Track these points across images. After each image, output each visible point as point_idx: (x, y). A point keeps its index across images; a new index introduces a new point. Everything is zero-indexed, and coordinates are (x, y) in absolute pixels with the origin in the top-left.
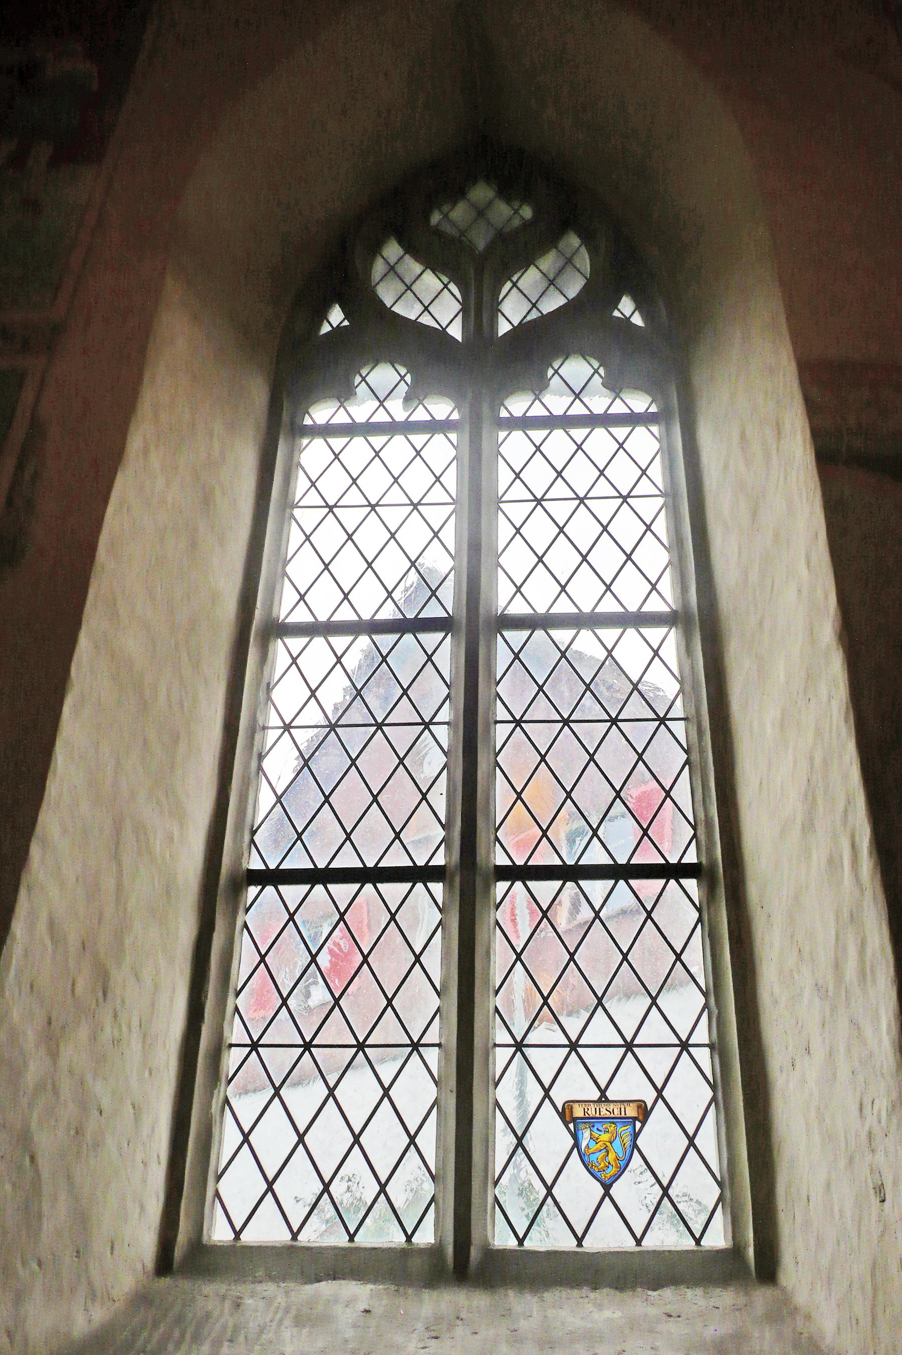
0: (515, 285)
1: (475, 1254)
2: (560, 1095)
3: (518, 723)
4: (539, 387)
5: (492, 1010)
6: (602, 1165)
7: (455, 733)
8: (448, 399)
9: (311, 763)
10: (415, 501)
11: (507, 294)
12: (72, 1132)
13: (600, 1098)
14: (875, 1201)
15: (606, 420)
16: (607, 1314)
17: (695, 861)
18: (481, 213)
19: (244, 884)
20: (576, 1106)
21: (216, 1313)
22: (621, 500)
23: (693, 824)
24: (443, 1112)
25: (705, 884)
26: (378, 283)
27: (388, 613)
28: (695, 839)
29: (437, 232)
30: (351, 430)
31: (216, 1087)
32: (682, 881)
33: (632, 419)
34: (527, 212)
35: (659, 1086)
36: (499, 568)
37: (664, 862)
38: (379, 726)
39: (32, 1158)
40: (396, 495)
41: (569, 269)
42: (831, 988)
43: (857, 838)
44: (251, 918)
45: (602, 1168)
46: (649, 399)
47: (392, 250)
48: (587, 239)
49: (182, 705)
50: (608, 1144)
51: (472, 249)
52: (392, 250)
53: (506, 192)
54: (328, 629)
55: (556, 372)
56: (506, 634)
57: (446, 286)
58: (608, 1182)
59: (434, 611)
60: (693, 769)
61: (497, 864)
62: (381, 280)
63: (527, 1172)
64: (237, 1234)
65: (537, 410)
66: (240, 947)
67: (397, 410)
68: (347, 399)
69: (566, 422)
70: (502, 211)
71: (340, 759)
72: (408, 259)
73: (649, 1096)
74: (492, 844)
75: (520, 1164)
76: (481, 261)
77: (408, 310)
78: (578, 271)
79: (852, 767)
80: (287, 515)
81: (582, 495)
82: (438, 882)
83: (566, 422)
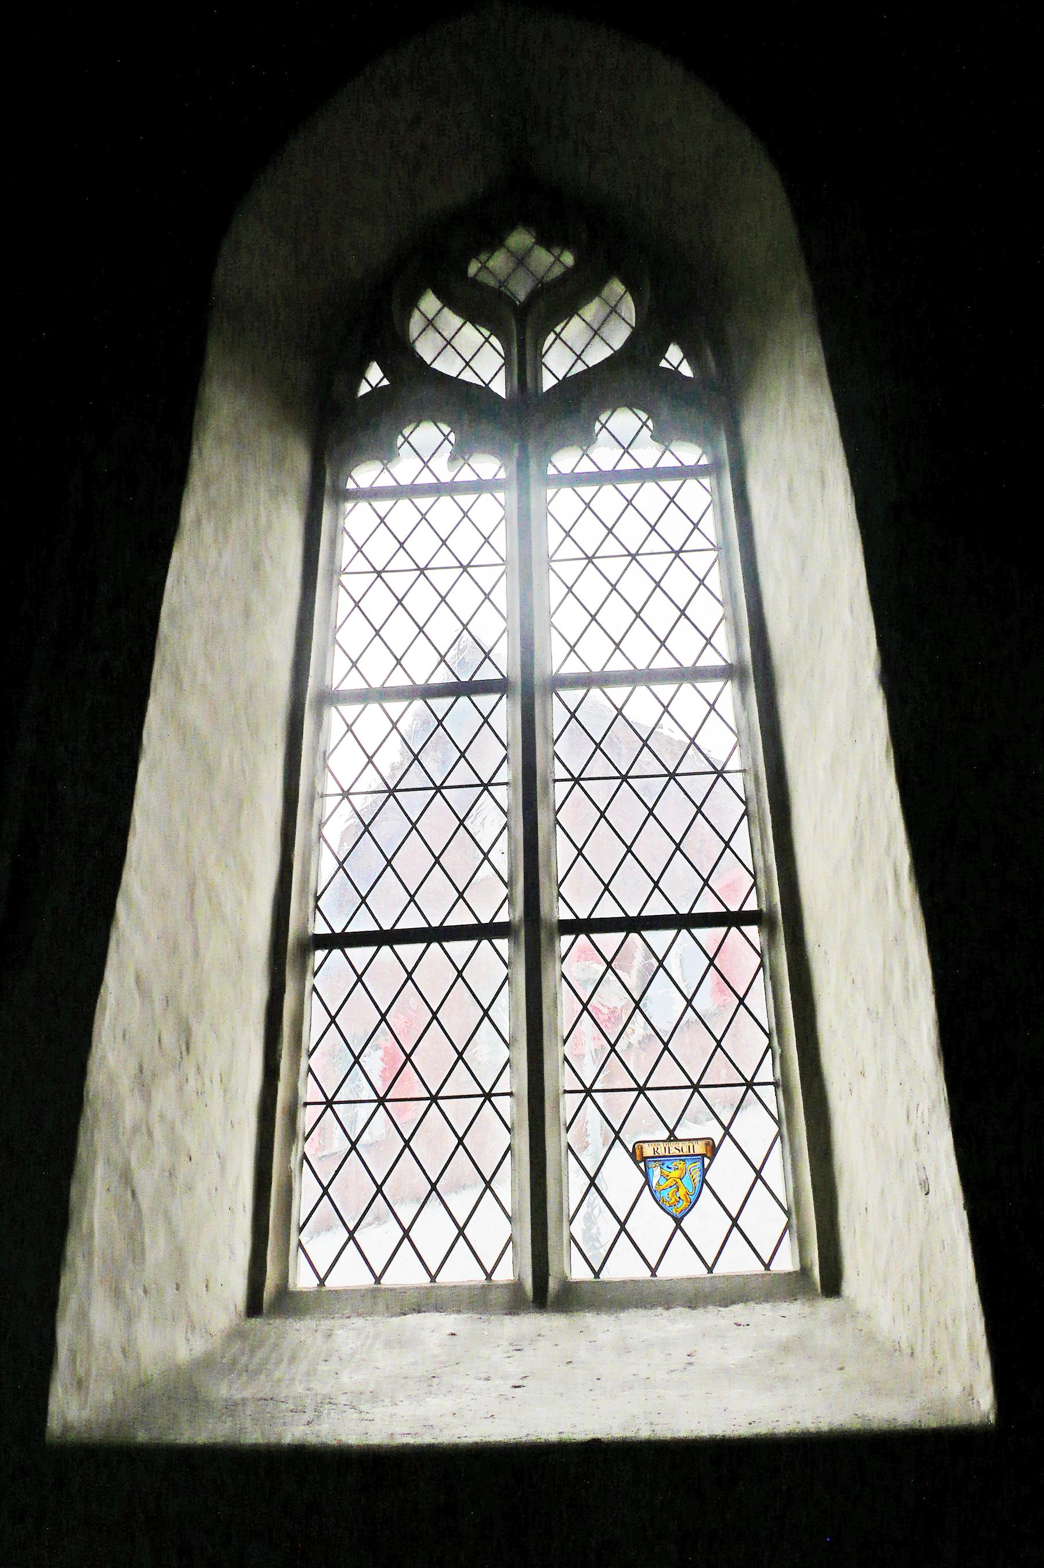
0: (558, 336)
1: (553, 1284)
2: (629, 1137)
3: (577, 780)
4: (587, 439)
5: (561, 1059)
6: (673, 1200)
7: (515, 790)
8: (492, 457)
9: (372, 828)
10: (465, 564)
11: (549, 349)
12: (167, 1174)
13: (669, 1137)
14: (921, 1194)
15: (657, 474)
16: (681, 1326)
17: (755, 908)
18: (521, 260)
19: (312, 947)
20: (645, 1145)
21: (309, 1342)
22: (673, 555)
23: (753, 873)
24: (517, 1157)
25: (765, 931)
26: (416, 339)
27: (443, 677)
28: (755, 888)
29: (474, 282)
30: (397, 492)
31: (294, 1142)
32: (743, 928)
33: (682, 473)
34: (568, 259)
35: (726, 1124)
36: (552, 628)
37: (725, 910)
38: (438, 789)
39: (134, 1193)
40: (444, 558)
41: (614, 316)
42: (880, 1011)
43: (898, 863)
44: (319, 981)
45: (673, 1203)
46: (699, 451)
47: (430, 303)
48: (632, 288)
49: (244, 772)
50: (678, 1180)
51: (509, 301)
52: (430, 303)
53: (545, 240)
54: (385, 694)
55: (604, 426)
56: (562, 693)
57: (487, 340)
58: (679, 1216)
59: (488, 673)
60: (752, 819)
61: (560, 918)
62: (419, 336)
63: (600, 1209)
64: (322, 1282)
65: (586, 466)
66: (310, 1009)
67: (442, 469)
68: (390, 460)
69: (615, 477)
70: (542, 258)
71: (400, 823)
72: (447, 313)
73: (717, 1134)
74: (555, 900)
75: (594, 1203)
76: (522, 312)
77: (448, 366)
78: (623, 319)
79: (893, 800)
80: (335, 582)
81: (633, 552)
82: (503, 938)
83: (615, 477)
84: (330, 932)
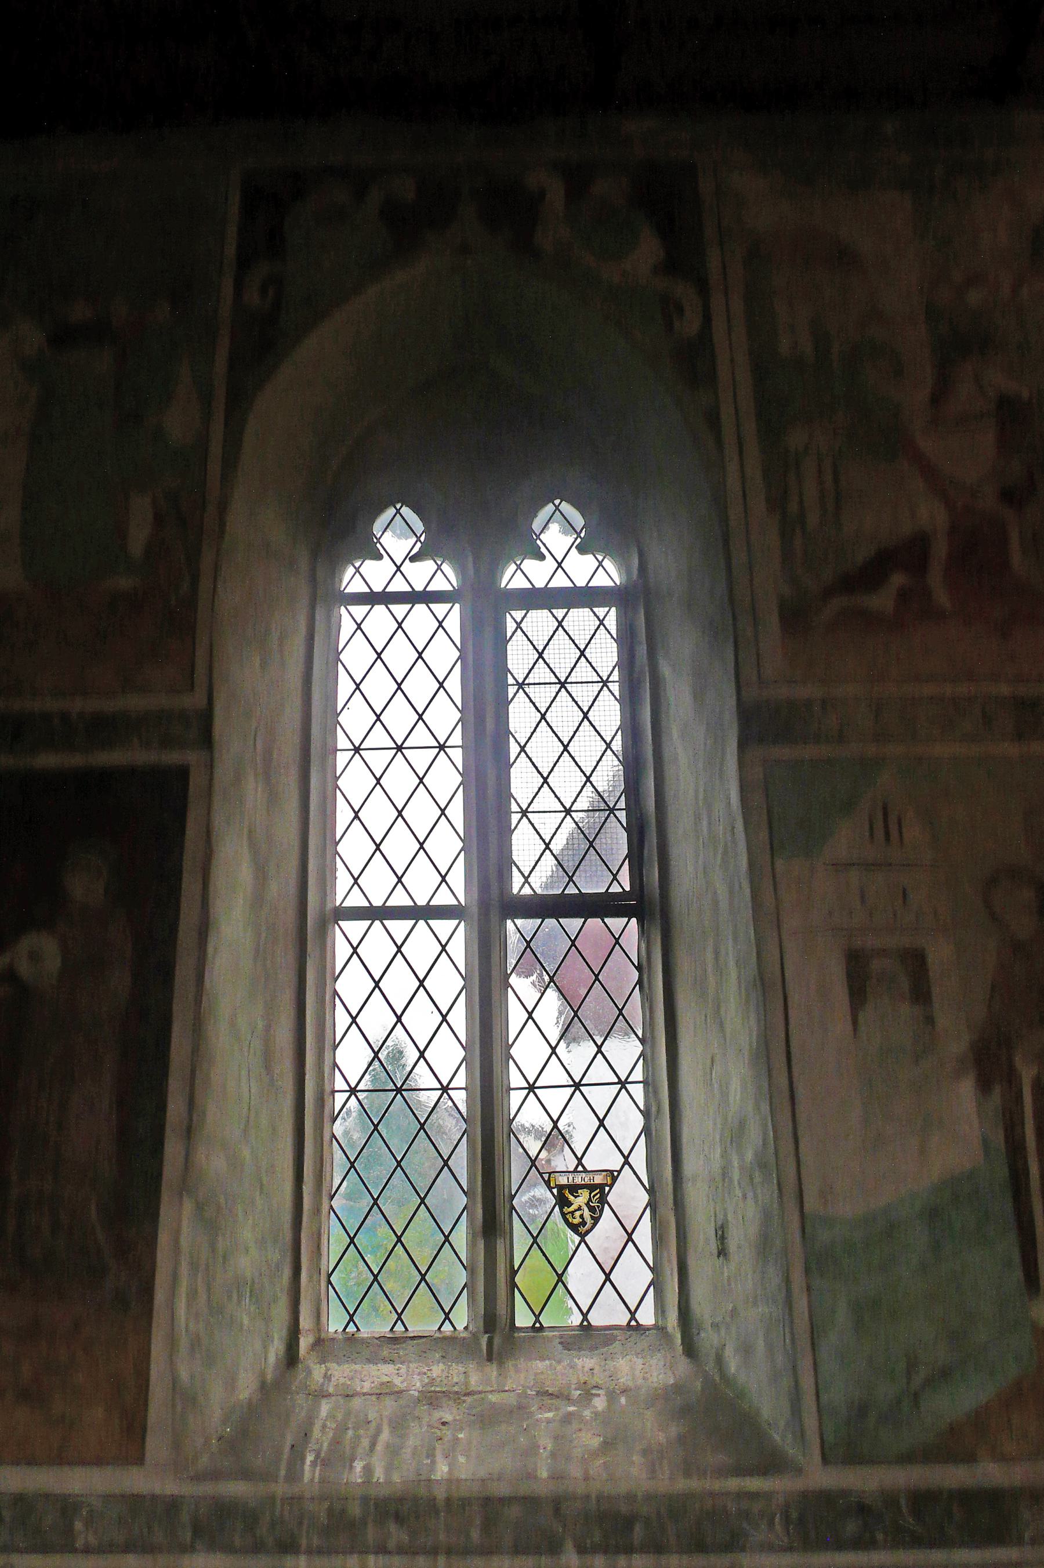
84: (369, 591)
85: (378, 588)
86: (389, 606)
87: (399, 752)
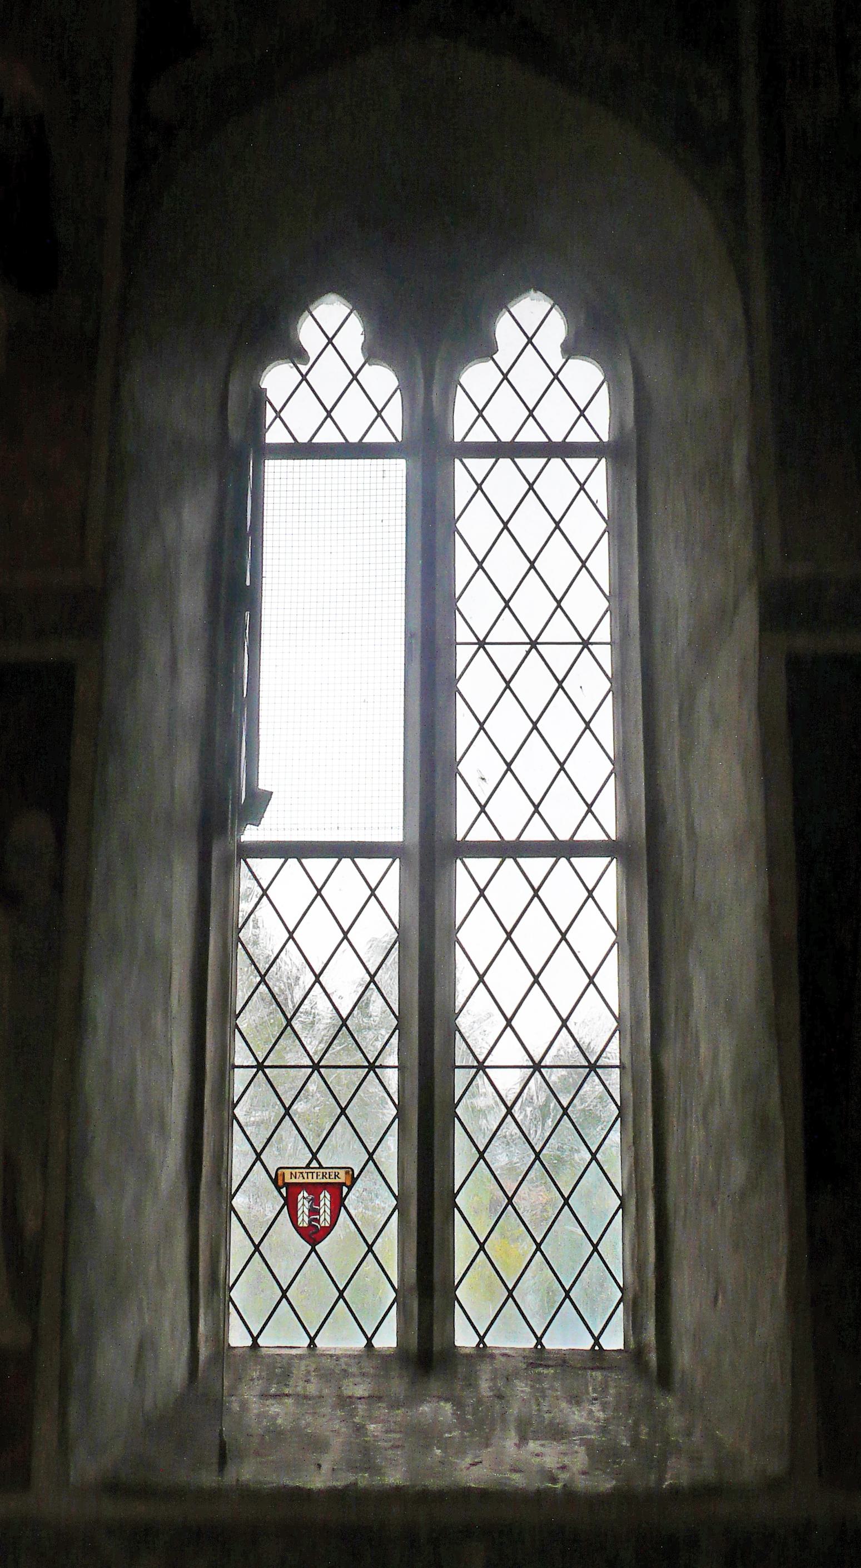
2: (272, 1160)
84: (292, 441)
85: (506, 437)
86: (516, 460)
87: (481, 650)
